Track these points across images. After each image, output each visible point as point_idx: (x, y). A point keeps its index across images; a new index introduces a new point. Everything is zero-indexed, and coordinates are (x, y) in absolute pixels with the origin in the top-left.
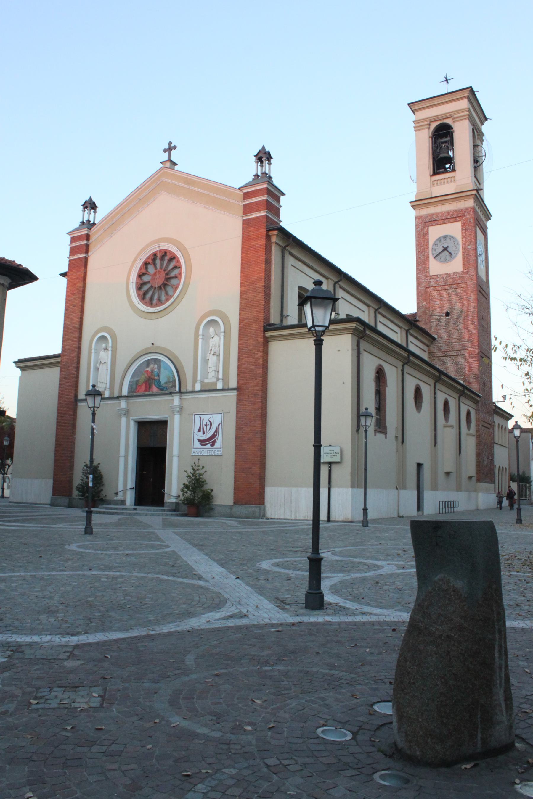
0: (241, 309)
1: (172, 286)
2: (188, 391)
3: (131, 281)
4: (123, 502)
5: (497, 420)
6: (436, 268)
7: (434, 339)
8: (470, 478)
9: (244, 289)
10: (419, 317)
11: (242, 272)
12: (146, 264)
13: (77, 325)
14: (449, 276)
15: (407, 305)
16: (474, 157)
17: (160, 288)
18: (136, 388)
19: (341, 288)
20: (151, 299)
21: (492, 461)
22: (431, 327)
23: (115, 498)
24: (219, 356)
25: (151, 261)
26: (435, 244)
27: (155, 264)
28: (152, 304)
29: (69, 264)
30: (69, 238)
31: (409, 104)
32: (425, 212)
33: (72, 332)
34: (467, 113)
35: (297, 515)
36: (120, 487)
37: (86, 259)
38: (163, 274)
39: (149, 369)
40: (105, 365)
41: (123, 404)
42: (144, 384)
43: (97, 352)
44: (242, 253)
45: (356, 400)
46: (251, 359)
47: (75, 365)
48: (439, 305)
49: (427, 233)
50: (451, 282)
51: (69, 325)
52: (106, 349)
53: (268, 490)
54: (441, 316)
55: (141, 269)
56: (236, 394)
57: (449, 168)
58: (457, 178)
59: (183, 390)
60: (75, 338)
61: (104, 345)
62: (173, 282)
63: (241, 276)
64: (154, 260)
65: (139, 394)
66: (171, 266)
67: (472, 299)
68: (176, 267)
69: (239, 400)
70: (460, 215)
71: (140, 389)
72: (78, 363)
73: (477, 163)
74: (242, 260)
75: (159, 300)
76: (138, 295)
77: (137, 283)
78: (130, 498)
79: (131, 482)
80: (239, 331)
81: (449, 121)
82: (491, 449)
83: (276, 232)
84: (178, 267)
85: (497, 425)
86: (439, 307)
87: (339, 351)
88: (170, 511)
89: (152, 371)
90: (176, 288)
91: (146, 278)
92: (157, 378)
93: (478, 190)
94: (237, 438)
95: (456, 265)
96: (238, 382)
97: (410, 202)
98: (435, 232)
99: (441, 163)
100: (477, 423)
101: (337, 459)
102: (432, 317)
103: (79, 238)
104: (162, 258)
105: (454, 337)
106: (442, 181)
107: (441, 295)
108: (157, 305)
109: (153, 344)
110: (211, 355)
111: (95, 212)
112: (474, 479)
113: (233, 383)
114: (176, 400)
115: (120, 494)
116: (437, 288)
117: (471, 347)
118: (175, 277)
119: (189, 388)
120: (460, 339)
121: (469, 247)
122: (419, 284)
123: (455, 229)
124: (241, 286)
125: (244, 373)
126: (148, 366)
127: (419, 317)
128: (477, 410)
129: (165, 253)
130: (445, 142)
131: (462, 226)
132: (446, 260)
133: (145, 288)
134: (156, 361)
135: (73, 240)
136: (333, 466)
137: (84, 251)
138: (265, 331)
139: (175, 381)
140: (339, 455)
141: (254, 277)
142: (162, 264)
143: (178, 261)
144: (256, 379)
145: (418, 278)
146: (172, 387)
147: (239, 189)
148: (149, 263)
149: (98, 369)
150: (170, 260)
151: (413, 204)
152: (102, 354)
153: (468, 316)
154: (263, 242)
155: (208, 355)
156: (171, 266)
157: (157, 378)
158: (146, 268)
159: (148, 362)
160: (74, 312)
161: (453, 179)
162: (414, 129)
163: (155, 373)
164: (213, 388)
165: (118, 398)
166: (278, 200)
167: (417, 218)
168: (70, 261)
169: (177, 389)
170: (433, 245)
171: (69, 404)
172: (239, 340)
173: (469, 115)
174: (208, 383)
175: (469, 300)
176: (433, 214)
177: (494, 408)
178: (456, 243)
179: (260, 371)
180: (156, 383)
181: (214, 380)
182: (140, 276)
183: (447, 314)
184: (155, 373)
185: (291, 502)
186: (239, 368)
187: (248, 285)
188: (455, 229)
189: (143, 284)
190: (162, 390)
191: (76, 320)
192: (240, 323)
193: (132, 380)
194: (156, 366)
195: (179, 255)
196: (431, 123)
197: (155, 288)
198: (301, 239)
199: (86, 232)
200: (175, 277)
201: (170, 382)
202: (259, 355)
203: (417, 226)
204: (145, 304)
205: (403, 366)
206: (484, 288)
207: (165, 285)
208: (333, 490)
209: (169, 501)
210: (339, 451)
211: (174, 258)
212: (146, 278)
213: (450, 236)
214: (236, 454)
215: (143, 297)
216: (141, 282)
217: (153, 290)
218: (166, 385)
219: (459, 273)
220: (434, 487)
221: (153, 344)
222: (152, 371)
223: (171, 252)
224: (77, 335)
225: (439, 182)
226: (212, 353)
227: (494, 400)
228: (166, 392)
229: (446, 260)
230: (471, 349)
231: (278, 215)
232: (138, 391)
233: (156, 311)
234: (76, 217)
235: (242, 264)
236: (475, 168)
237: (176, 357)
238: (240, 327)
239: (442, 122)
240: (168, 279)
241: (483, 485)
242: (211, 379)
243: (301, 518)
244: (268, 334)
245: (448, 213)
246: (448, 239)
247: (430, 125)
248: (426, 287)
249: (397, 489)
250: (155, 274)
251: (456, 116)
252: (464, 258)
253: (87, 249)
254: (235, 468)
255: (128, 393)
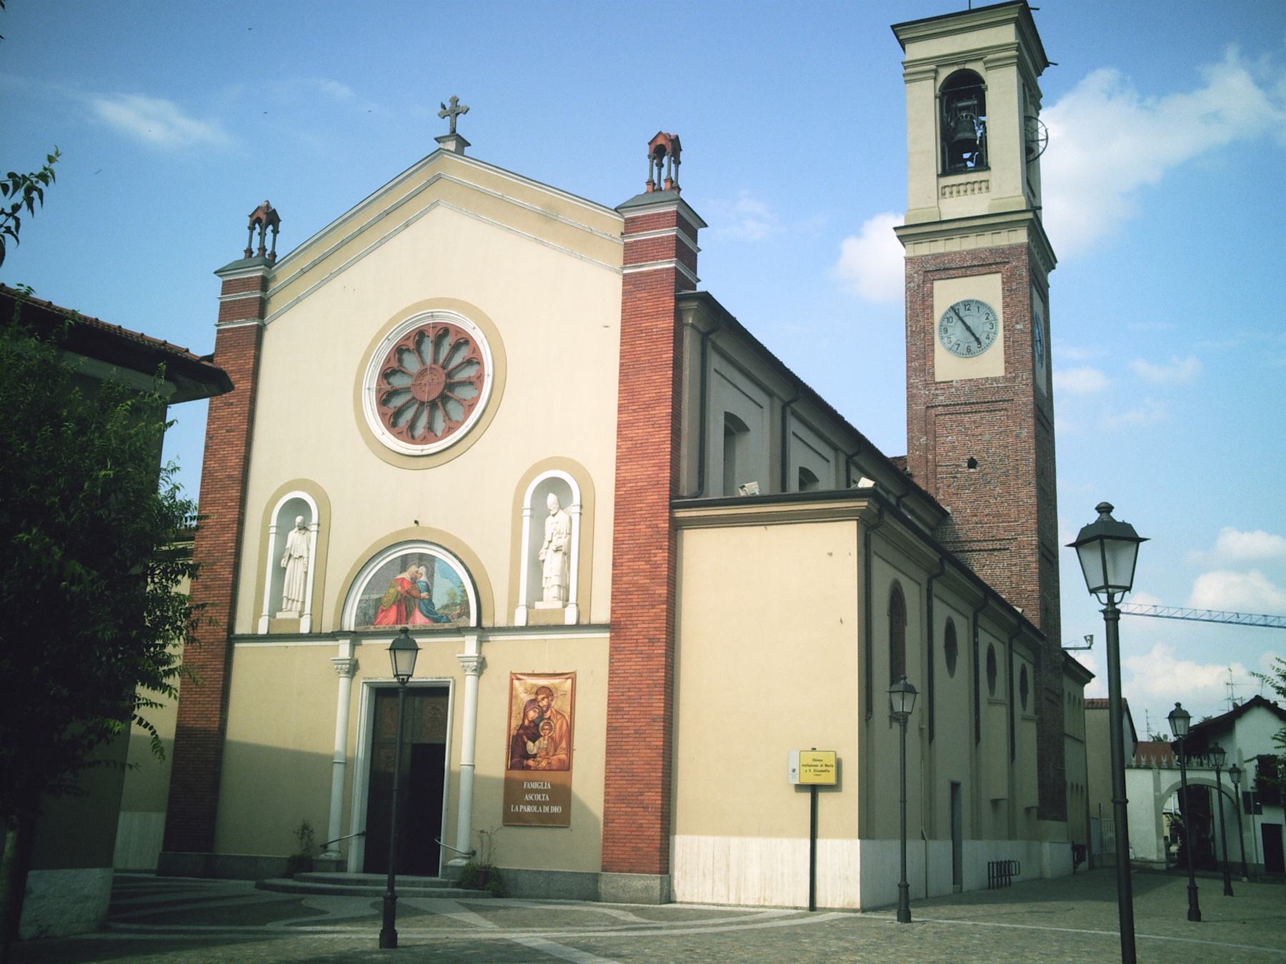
0: (619, 459)
1: (460, 402)
2: (497, 625)
3: (366, 384)
4: (341, 865)
5: (1068, 685)
6: (949, 366)
7: (945, 514)
8: (1028, 810)
9: (626, 417)
10: (912, 467)
11: (621, 382)
12: (399, 351)
13: (236, 473)
14: (976, 385)
15: (891, 439)
16: (1027, 142)
17: (433, 405)
18: (376, 615)
19: (795, 414)
20: (412, 426)
21: (1062, 773)
22: (937, 489)
23: (322, 856)
24: (567, 554)
25: (412, 346)
26: (946, 318)
27: (419, 351)
28: (413, 437)
29: (218, 339)
30: (219, 282)
31: (893, 27)
32: (925, 249)
33: (223, 488)
34: (1014, 53)
35: (743, 897)
36: (333, 834)
37: (260, 331)
38: (443, 373)
39: (406, 575)
40: (300, 563)
41: (344, 647)
42: (395, 608)
43: (282, 534)
44: (622, 344)
45: (926, 671)
46: (642, 565)
47: (231, 559)
48: (953, 442)
49: (931, 294)
50: (978, 400)
51: (217, 471)
52: (304, 528)
53: (684, 846)
54: (958, 466)
55: (388, 360)
56: (608, 635)
57: (970, 159)
58: (993, 184)
59: (486, 623)
60: (232, 501)
61: (299, 519)
62: (465, 393)
63: (620, 392)
64: (419, 343)
65: (381, 628)
66: (458, 359)
67: (1024, 433)
68: (469, 362)
69: (614, 650)
70: (998, 260)
71: (385, 617)
72: (238, 554)
73: (1030, 153)
74: (622, 357)
75: (430, 427)
76: (383, 415)
77: (378, 391)
78: (354, 858)
79: (357, 822)
80: (616, 504)
81: (978, 67)
82: (1061, 750)
83: (694, 305)
84: (474, 361)
85: (1066, 694)
86: (954, 448)
87: (831, 554)
88: (458, 885)
89: (414, 580)
90: (471, 406)
91: (398, 382)
92: (424, 595)
93: (1035, 209)
94: (611, 729)
95: (991, 364)
96: (613, 612)
97: (895, 229)
98: (947, 293)
99: (961, 150)
100: (1037, 697)
101: (830, 779)
102: (939, 469)
103: (244, 285)
104: (437, 344)
105: (987, 511)
106: (962, 188)
107: (961, 423)
108: (425, 440)
109: (416, 522)
110: (550, 551)
111: (276, 232)
112: (1034, 812)
113: (602, 612)
114: (470, 644)
115: (334, 846)
116: (951, 409)
117: (1022, 534)
118: (469, 383)
119: (501, 621)
120: (998, 515)
121: (1018, 327)
122: (911, 398)
123: (989, 289)
124: (620, 412)
125: (628, 593)
126: (404, 568)
127: (912, 467)
128: (1037, 666)
129: (444, 331)
130: (967, 108)
131: (1003, 283)
132: (969, 350)
133: (398, 402)
134: (422, 559)
135: (227, 287)
136: (823, 798)
137: (256, 313)
138: (673, 507)
139: (467, 603)
140: (833, 770)
141: (649, 395)
142: (449, 358)
143: (476, 349)
144: (653, 607)
145: (910, 387)
146: (460, 616)
147: (616, 210)
148: (408, 350)
149: (285, 569)
150: (456, 347)
151: (902, 232)
152: (294, 536)
153: (1016, 468)
154: (668, 323)
155: (543, 550)
156: (458, 359)
157: (424, 595)
158: (400, 360)
159: (405, 562)
160: (230, 443)
161: (984, 185)
162: (903, 79)
163: (421, 585)
164: (553, 622)
165: (334, 636)
166: (694, 236)
167: (909, 261)
168: (219, 332)
169: (473, 623)
170: (943, 319)
171: (212, 644)
172: (616, 524)
173: (1017, 57)
174: (545, 612)
175: (1017, 436)
176: (943, 255)
177: (1063, 659)
178: (991, 318)
179: (663, 591)
180: (423, 608)
181: (559, 605)
182: (386, 374)
183: (972, 463)
184: (421, 585)
185: (728, 866)
186: (614, 582)
187: (634, 411)
188: (989, 289)
189: (394, 393)
190: (437, 621)
191: (234, 461)
192: (617, 488)
193: (366, 597)
194: (422, 569)
195: (478, 336)
196: (940, 70)
197: (422, 403)
198: (733, 314)
199: (260, 274)
200: (469, 383)
201: (455, 604)
202: (661, 556)
203: (909, 278)
204: (399, 435)
205: (929, 582)
206: (1045, 410)
207: (444, 398)
208: (819, 842)
209: (451, 862)
210: (833, 763)
211: (464, 341)
212: (398, 382)
213: (977, 302)
214: (608, 763)
215: (392, 421)
216: (388, 388)
217: (416, 406)
218: (447, 612)
219: (996, 380)
220: (977, 835)
221: (416, 522)
222: (414, 580)
223: (459, 330)
224: (235, 493)
225: (955, 189)
226: (553, 547)
227: (1064, 645)
228: (447, 626)
229: (969, 350)
230: (1020, 538)
231: (693, 267)
232: (380, 623)
233: (425, 453)
234: (234, 242)
235: (622, 365)
236: (1028, 162)
237: (468, 550)
238: (617, 497)
239: (961, 67)
240: (450, 386)
241: (1052, 826)
242: (550, 601)
243: (751, 903)
244: (681, 514)
245: (974, 253)
246: (974, 308)
247: (936, 72)
248: (929, 406)
249: (923, 838)
250: (422, 373)
251: (990, 57)
252: (1007, 347)
253: (261, 308)
254: (607, 794)
255: (356, 625)
